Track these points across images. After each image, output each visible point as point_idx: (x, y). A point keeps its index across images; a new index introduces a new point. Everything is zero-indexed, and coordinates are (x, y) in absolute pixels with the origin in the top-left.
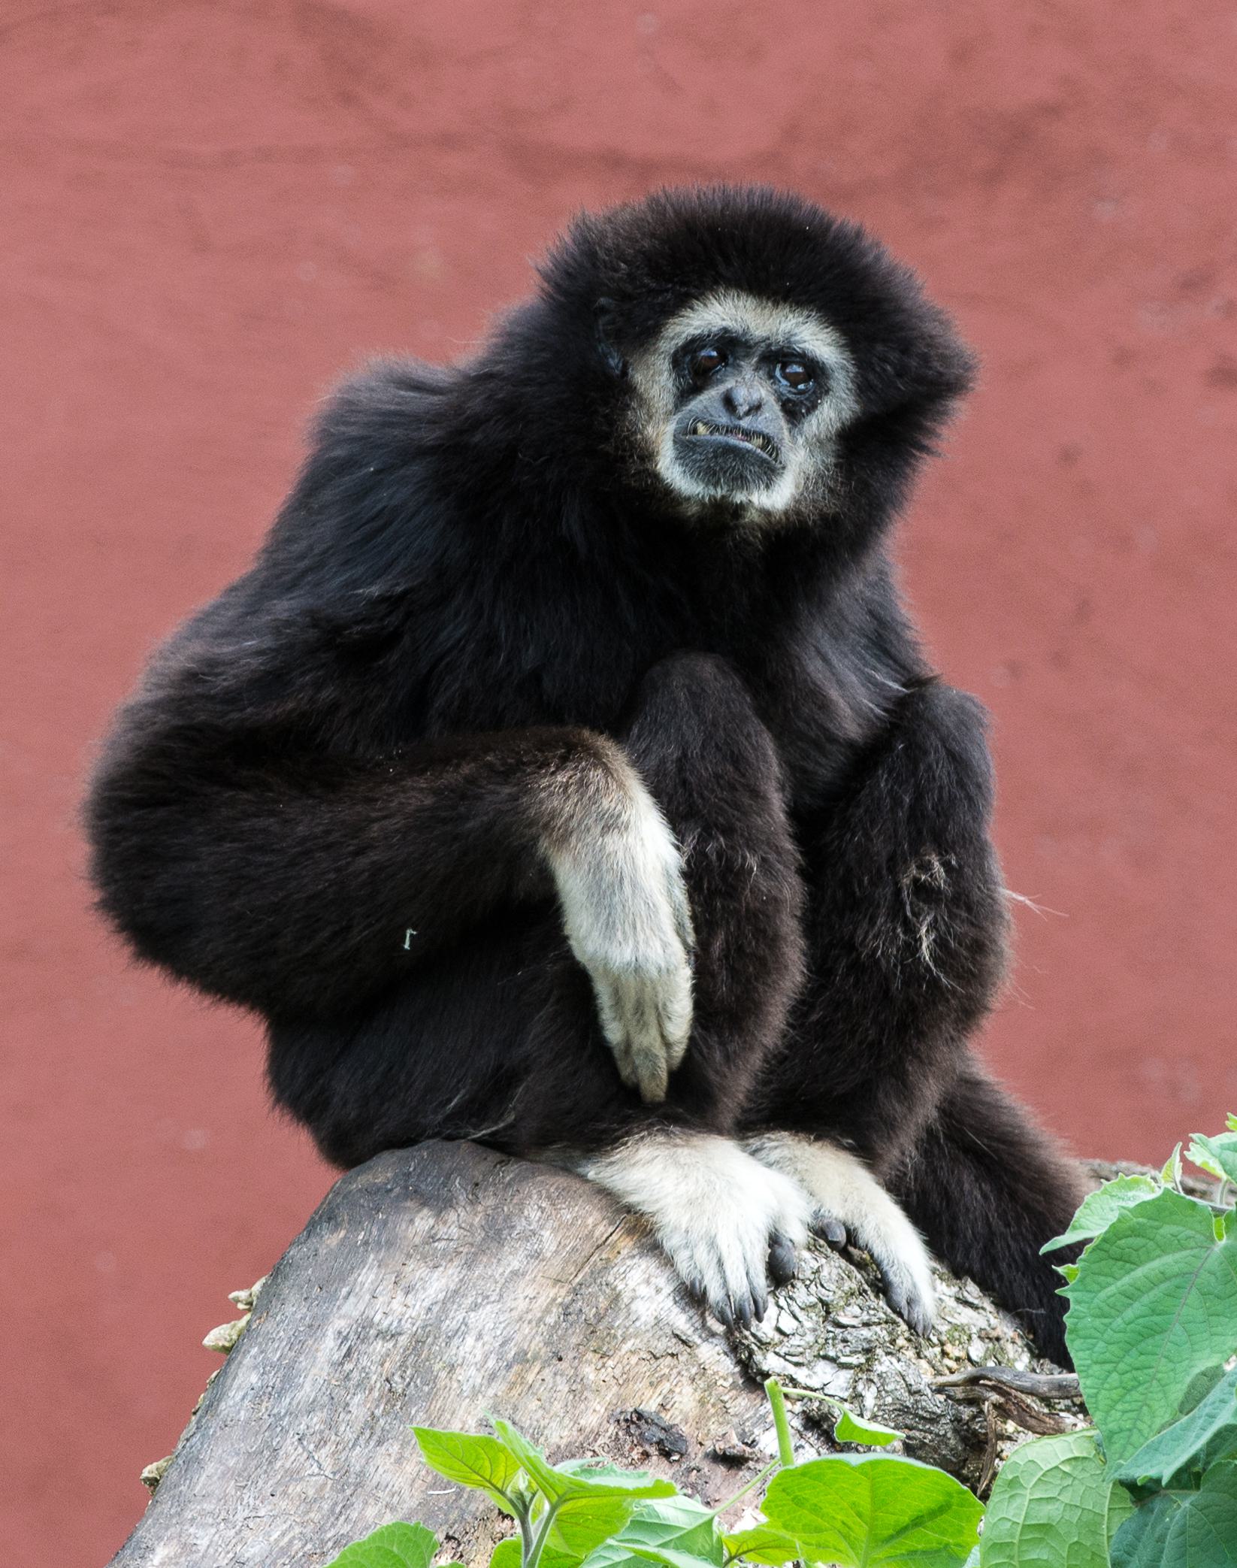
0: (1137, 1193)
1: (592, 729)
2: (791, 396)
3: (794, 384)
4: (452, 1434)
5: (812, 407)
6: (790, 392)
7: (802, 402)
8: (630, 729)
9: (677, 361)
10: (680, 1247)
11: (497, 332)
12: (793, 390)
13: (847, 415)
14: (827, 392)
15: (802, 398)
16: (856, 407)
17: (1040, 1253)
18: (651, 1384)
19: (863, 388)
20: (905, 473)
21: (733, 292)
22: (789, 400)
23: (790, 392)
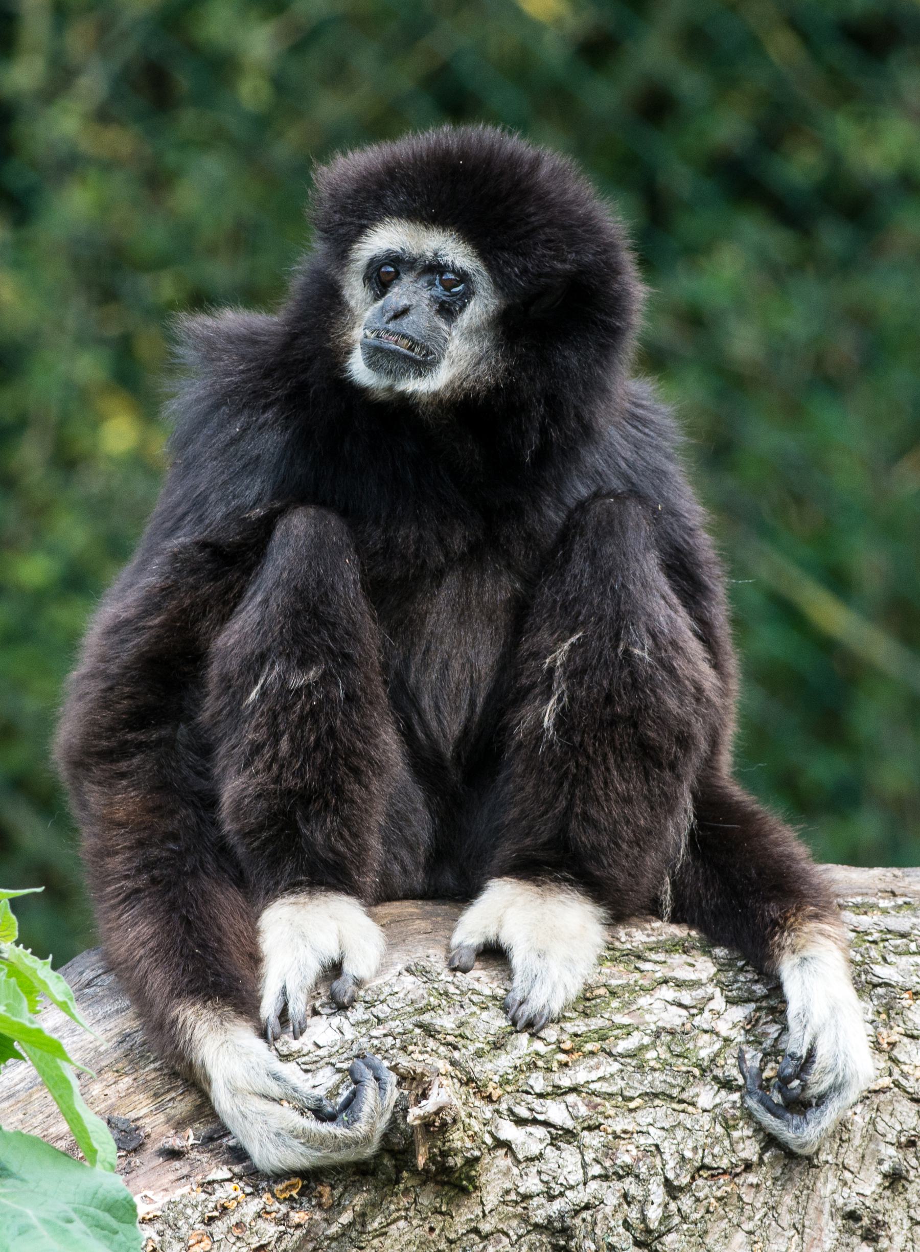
0: (647, 940)
2: (444, 298)
3: (447, 289)
4: (40, 1031)
5: (463, 308)
6: (444, 295)
7: (455, 302)
8: (597, 876)
9: (367, 278)
12: (448, 294)
13: (492, 308)
14: (474, 293)
15: (454, 298)
16: (497, 302)
17: (43, 888)
18: (155, 1095)
19: (501, 283)
20: (436, 144)
21: (395, 220)
22: (444, 302)
23: (444, 295)
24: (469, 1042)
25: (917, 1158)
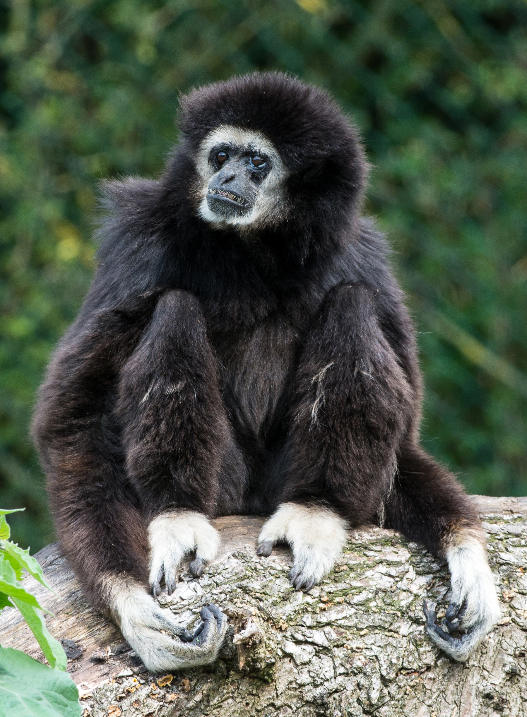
0: (371, 538)
1: (454, 638)
2: (254, 171)
3: (256, 165)
4: (23, 590)
5: (265, 176)
6: (254, 169)
7: (260, 173)
9: (210, 159)
10: (228, 615)
11: (485, 617)
12: (257, 168)
13: (282, 176)
14: (271, 168)
15: (260, 171)
16: (285, 173)
17: (25, 508)
18: (89, 627)
19: (287, 162)
21: (226, 126)
22: (254, 173)
23: (254, 169)
24: (268, 597)
25: (525, 663)
